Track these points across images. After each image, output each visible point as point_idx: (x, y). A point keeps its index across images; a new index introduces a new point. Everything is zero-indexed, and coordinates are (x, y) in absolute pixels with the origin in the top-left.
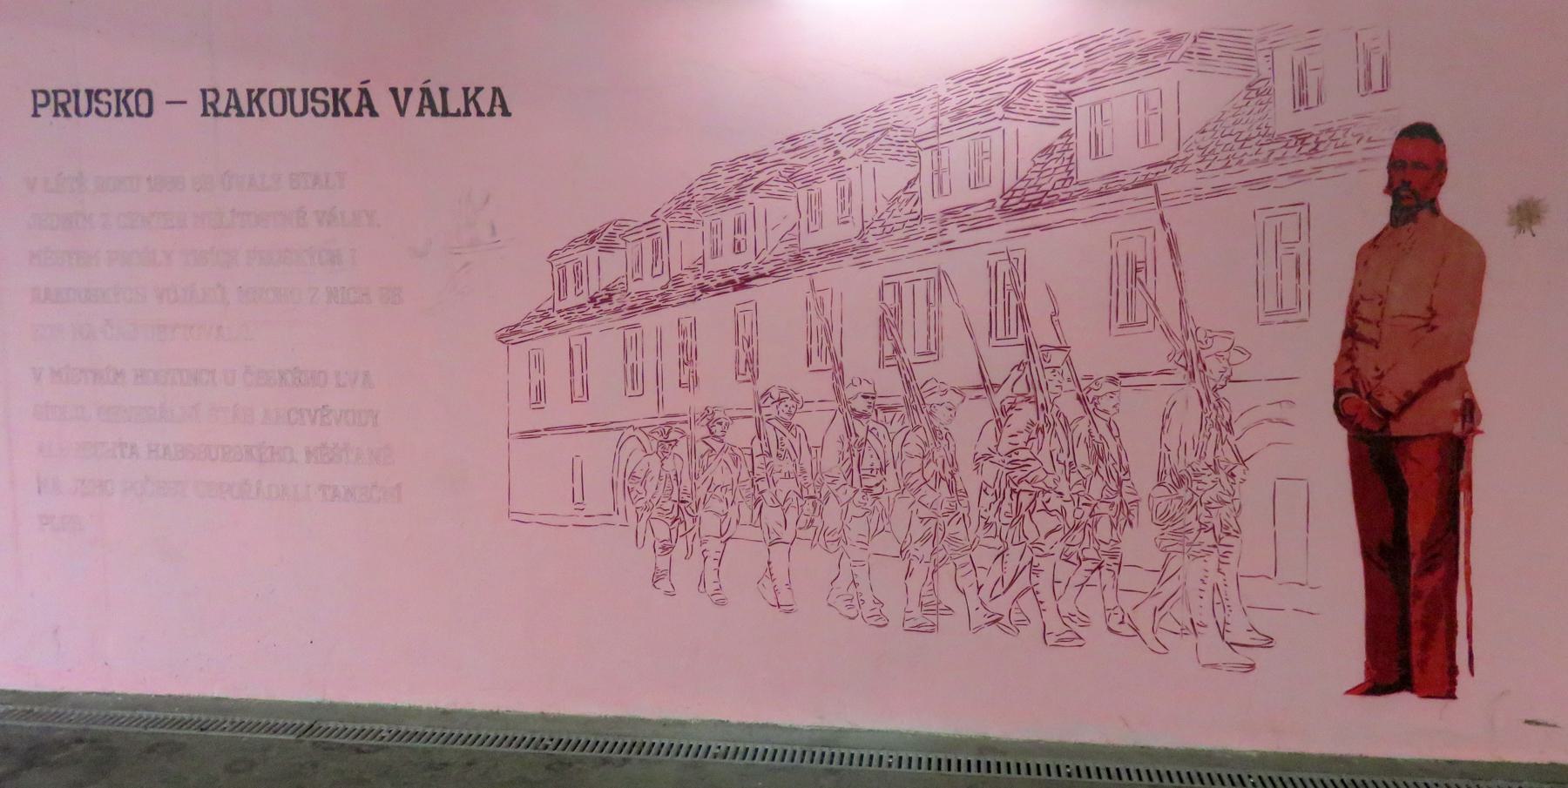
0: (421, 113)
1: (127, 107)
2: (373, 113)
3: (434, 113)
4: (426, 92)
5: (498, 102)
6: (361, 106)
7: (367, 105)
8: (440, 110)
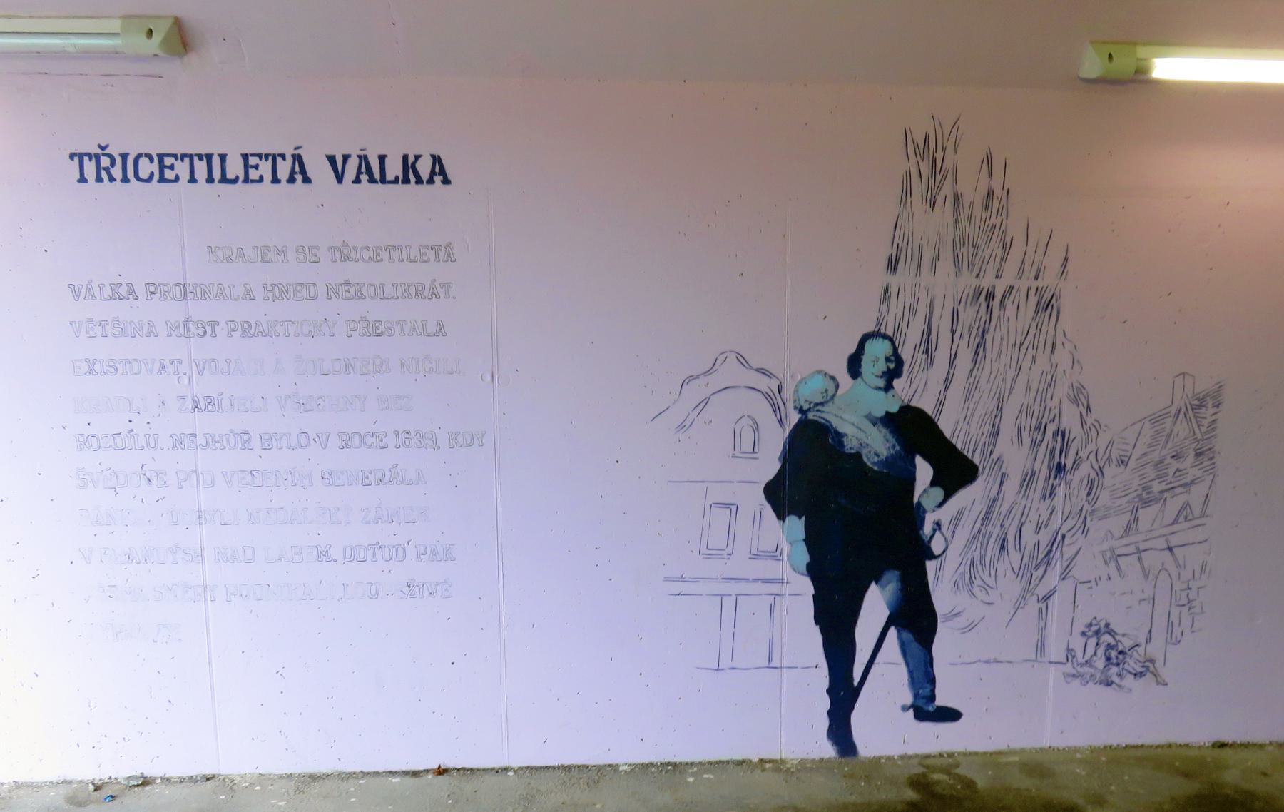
0: (357, 181)
1: (416, 174)
2: (446, 181)
3: (372, 180)
4: (363, 159)
5: (363, 169)
6: (433, 173)
7: (300, 172)
8: (377, 175)
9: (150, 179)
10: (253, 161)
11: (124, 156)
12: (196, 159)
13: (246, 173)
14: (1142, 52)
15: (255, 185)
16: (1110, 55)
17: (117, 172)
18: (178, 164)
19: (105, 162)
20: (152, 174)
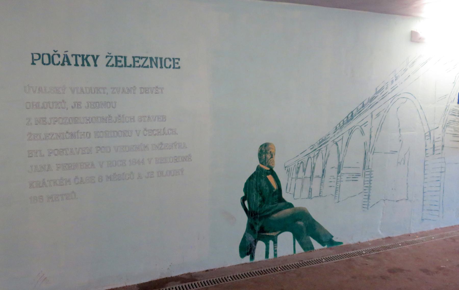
5: (66, 60)
10: (136, 59)
12: (78, 56)
13: (116, 63)
15: (138, 68)
20: (170, 66)
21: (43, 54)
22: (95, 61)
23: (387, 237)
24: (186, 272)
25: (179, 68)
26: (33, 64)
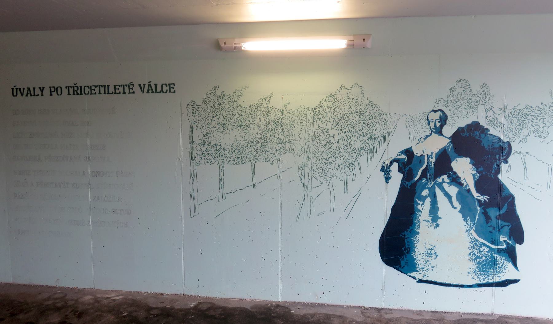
0: (27, 96)
4: (29, 89)
9: (166, 92)
10: (117, 87)
11: (81, 87)
14: (236, 41)
16: (364, 39)
17: (79, 92)
18: (120, 88)
19: (76, 89)
21: (57, 88)
22: (42, 91)
23: (433, 310)
24: (224, 297)
25: (174, 92)
26: (51, 95)
